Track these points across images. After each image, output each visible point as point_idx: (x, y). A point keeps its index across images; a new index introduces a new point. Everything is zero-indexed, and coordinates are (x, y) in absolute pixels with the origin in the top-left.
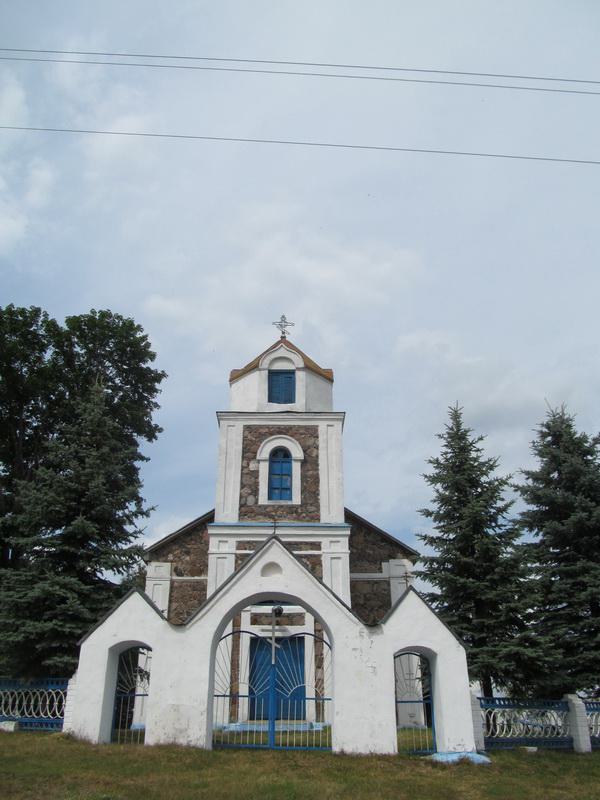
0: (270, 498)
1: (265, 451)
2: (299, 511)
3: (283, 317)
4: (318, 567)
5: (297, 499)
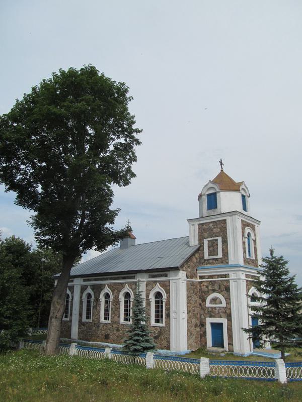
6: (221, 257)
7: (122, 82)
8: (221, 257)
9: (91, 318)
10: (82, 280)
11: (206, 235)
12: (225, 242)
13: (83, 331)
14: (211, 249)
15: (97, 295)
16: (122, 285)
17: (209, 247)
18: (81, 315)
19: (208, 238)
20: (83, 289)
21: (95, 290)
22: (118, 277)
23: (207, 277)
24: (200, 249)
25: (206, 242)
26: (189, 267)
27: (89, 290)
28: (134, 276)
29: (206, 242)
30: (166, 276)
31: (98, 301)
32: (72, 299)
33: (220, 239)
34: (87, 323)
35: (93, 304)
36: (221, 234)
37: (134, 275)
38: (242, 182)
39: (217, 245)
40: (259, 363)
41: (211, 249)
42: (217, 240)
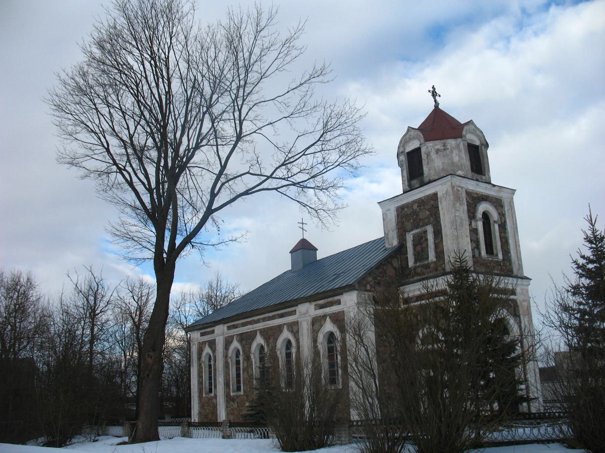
0: (487, 253)
1: (483, 207)
2: (502, 264)
3: (433, 86)
4: (516, 307)
5: (500, 256)
6: (434, 260)
7: (74, 167)
8: (434, 260)
9: (213, 391)
10: (199, 335)
11: (408, 225)
12: (438, 233)
13: (233, 409)
14: (419, 248)
15: (247, 349)
16: (279, 329)
17: (415, 246)
18: (227, 384)
19: (412, 230)
20: (228, 342)
21: (244, 342)
22: (273, 316)
23: (415, 299)
24: (401, 248)
25: (409, 237)
26: (379, 283)
27: (236, 344)
28: (214, 331)
29: (409, 237)
30: (339, 303)
31: (249, 360)
32: (298, 347)
33: (430, 229)
34: (238, 397)
35: (243, 365)
36: (432, 219)
37: (336, 298)
38: (470, 121)
39: (427, 240)
40: (530, 418)
41: (419, 248)
42: (426, 232)
